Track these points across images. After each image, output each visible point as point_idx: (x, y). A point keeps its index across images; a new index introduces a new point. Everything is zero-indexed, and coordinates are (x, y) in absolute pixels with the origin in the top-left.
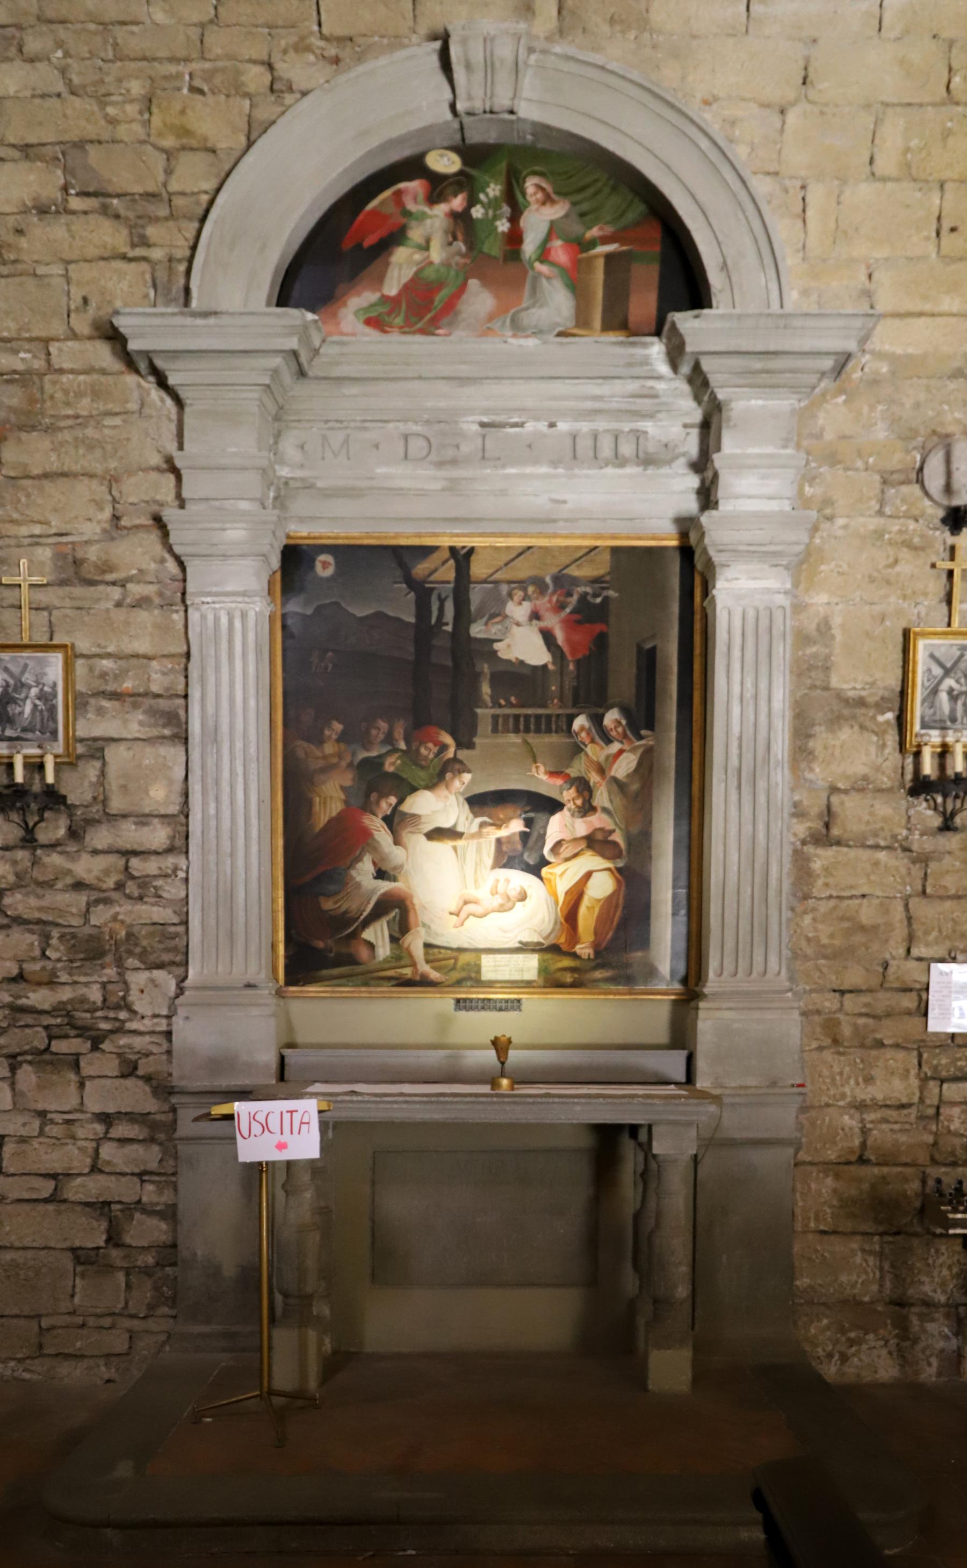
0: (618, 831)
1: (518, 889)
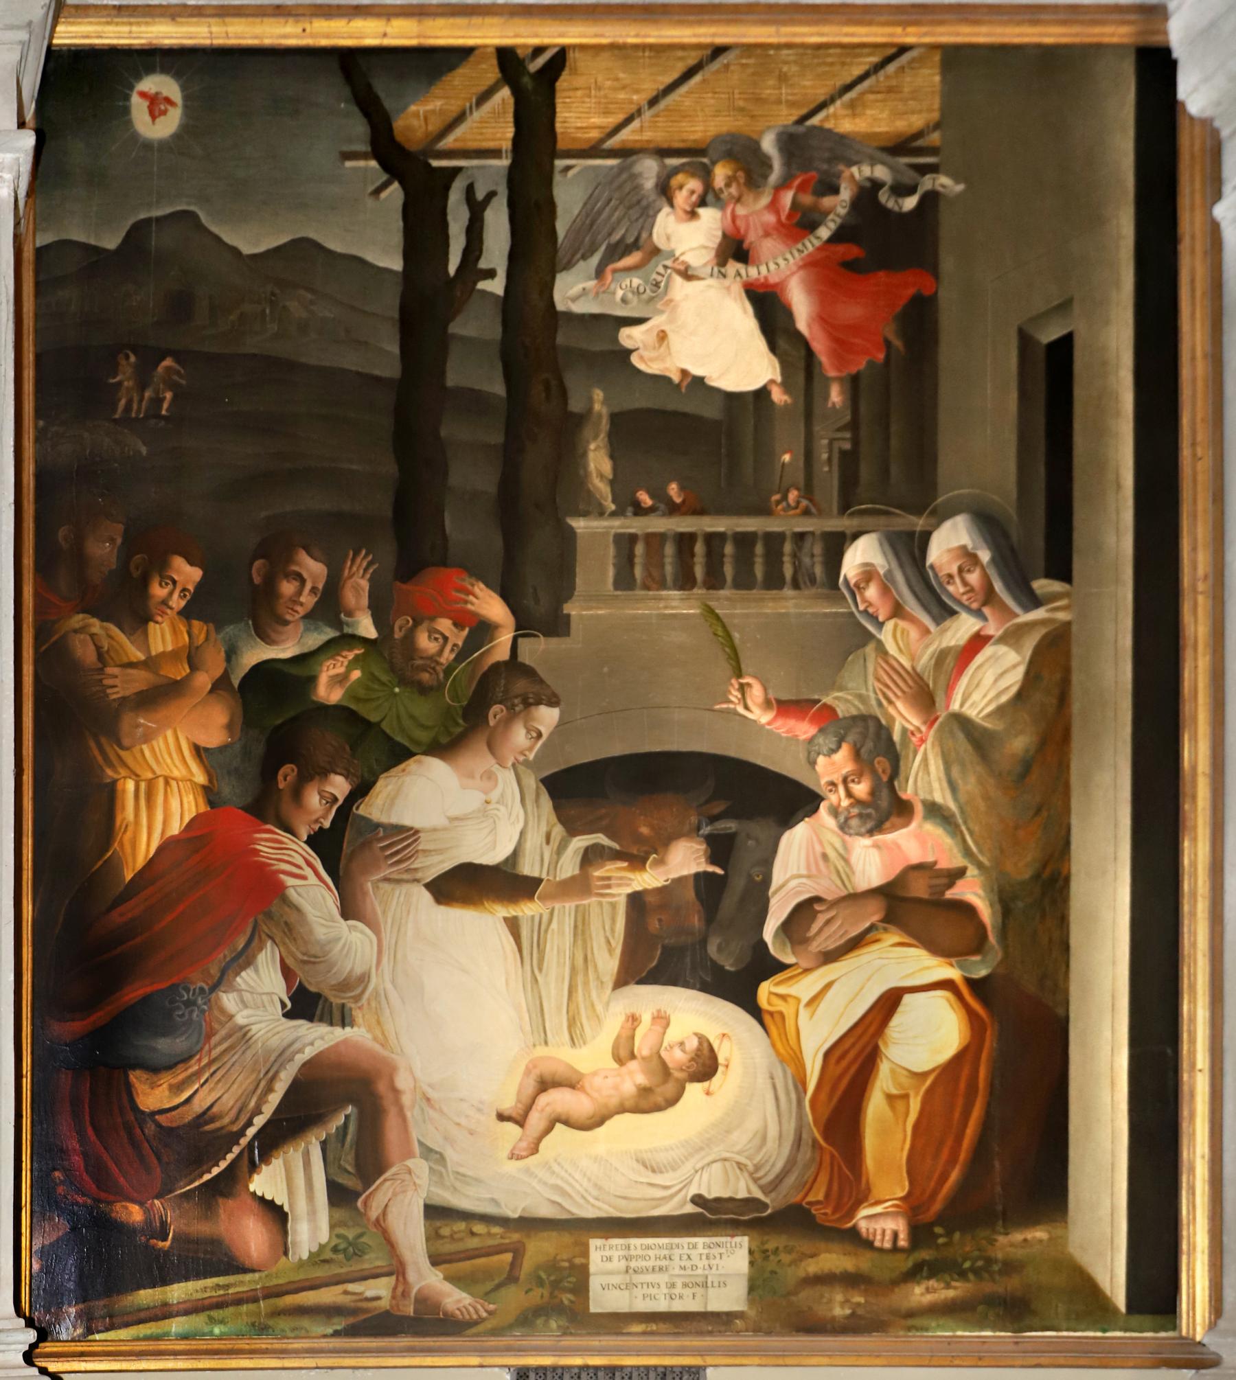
0: (972, 871)
1: (693, 1044)
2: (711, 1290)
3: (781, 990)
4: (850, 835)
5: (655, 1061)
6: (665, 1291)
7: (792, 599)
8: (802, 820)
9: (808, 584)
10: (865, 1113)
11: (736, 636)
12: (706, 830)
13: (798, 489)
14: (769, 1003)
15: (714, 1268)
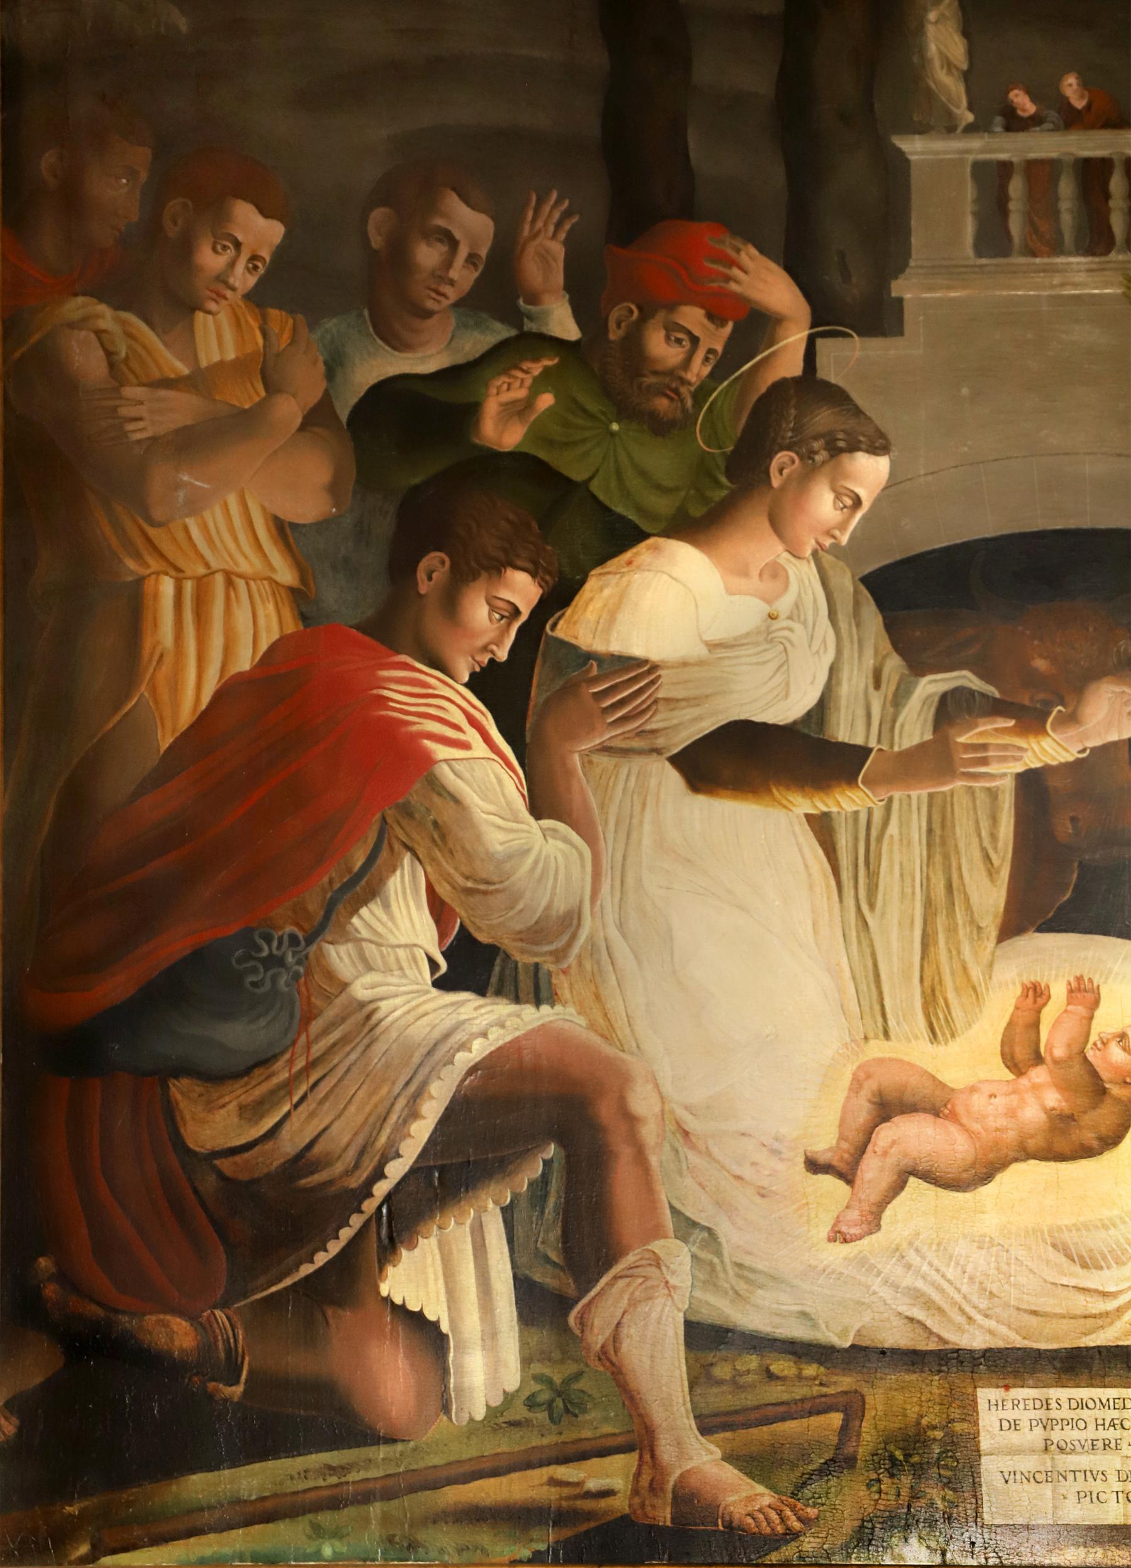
5: (1077, 1068)
6: (1118, 1487)
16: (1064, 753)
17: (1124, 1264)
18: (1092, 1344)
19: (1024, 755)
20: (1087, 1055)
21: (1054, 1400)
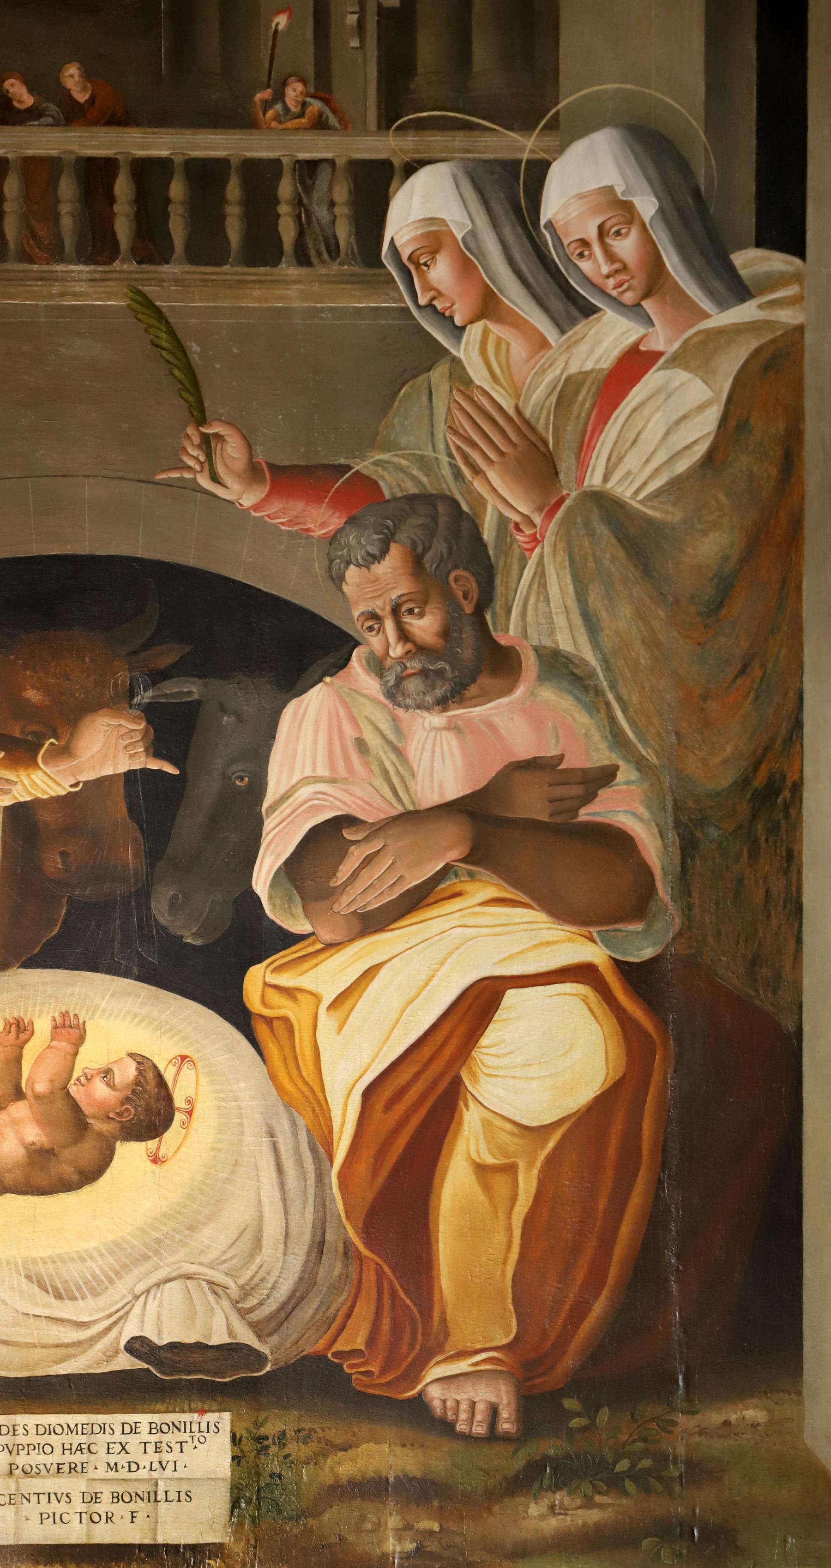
0: (626, 773)
1: (128, 1072)
2: (163, 1506)
3: (285, 980)
4: (407, 707)
5: (60, 1104)
6: (81, 1507)
7: (299, 282)
8: (320, 680)
9: (325, 256)
10: (440, 1195)
11: (194, 348)
12: (145, 696)
13: (303, 81)
14: (264, 1002)
15: (170, 1467)
16: (55, 787)
17: (99, 1294)
18: (62, 1372)
19: (13, 788)
20: (70, 1090)
21: (21, 1426)
